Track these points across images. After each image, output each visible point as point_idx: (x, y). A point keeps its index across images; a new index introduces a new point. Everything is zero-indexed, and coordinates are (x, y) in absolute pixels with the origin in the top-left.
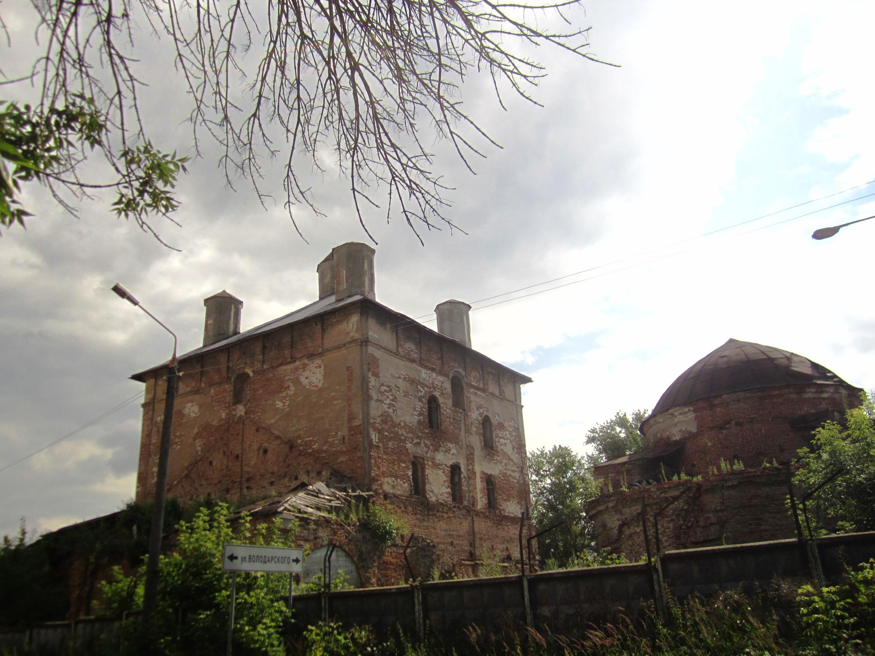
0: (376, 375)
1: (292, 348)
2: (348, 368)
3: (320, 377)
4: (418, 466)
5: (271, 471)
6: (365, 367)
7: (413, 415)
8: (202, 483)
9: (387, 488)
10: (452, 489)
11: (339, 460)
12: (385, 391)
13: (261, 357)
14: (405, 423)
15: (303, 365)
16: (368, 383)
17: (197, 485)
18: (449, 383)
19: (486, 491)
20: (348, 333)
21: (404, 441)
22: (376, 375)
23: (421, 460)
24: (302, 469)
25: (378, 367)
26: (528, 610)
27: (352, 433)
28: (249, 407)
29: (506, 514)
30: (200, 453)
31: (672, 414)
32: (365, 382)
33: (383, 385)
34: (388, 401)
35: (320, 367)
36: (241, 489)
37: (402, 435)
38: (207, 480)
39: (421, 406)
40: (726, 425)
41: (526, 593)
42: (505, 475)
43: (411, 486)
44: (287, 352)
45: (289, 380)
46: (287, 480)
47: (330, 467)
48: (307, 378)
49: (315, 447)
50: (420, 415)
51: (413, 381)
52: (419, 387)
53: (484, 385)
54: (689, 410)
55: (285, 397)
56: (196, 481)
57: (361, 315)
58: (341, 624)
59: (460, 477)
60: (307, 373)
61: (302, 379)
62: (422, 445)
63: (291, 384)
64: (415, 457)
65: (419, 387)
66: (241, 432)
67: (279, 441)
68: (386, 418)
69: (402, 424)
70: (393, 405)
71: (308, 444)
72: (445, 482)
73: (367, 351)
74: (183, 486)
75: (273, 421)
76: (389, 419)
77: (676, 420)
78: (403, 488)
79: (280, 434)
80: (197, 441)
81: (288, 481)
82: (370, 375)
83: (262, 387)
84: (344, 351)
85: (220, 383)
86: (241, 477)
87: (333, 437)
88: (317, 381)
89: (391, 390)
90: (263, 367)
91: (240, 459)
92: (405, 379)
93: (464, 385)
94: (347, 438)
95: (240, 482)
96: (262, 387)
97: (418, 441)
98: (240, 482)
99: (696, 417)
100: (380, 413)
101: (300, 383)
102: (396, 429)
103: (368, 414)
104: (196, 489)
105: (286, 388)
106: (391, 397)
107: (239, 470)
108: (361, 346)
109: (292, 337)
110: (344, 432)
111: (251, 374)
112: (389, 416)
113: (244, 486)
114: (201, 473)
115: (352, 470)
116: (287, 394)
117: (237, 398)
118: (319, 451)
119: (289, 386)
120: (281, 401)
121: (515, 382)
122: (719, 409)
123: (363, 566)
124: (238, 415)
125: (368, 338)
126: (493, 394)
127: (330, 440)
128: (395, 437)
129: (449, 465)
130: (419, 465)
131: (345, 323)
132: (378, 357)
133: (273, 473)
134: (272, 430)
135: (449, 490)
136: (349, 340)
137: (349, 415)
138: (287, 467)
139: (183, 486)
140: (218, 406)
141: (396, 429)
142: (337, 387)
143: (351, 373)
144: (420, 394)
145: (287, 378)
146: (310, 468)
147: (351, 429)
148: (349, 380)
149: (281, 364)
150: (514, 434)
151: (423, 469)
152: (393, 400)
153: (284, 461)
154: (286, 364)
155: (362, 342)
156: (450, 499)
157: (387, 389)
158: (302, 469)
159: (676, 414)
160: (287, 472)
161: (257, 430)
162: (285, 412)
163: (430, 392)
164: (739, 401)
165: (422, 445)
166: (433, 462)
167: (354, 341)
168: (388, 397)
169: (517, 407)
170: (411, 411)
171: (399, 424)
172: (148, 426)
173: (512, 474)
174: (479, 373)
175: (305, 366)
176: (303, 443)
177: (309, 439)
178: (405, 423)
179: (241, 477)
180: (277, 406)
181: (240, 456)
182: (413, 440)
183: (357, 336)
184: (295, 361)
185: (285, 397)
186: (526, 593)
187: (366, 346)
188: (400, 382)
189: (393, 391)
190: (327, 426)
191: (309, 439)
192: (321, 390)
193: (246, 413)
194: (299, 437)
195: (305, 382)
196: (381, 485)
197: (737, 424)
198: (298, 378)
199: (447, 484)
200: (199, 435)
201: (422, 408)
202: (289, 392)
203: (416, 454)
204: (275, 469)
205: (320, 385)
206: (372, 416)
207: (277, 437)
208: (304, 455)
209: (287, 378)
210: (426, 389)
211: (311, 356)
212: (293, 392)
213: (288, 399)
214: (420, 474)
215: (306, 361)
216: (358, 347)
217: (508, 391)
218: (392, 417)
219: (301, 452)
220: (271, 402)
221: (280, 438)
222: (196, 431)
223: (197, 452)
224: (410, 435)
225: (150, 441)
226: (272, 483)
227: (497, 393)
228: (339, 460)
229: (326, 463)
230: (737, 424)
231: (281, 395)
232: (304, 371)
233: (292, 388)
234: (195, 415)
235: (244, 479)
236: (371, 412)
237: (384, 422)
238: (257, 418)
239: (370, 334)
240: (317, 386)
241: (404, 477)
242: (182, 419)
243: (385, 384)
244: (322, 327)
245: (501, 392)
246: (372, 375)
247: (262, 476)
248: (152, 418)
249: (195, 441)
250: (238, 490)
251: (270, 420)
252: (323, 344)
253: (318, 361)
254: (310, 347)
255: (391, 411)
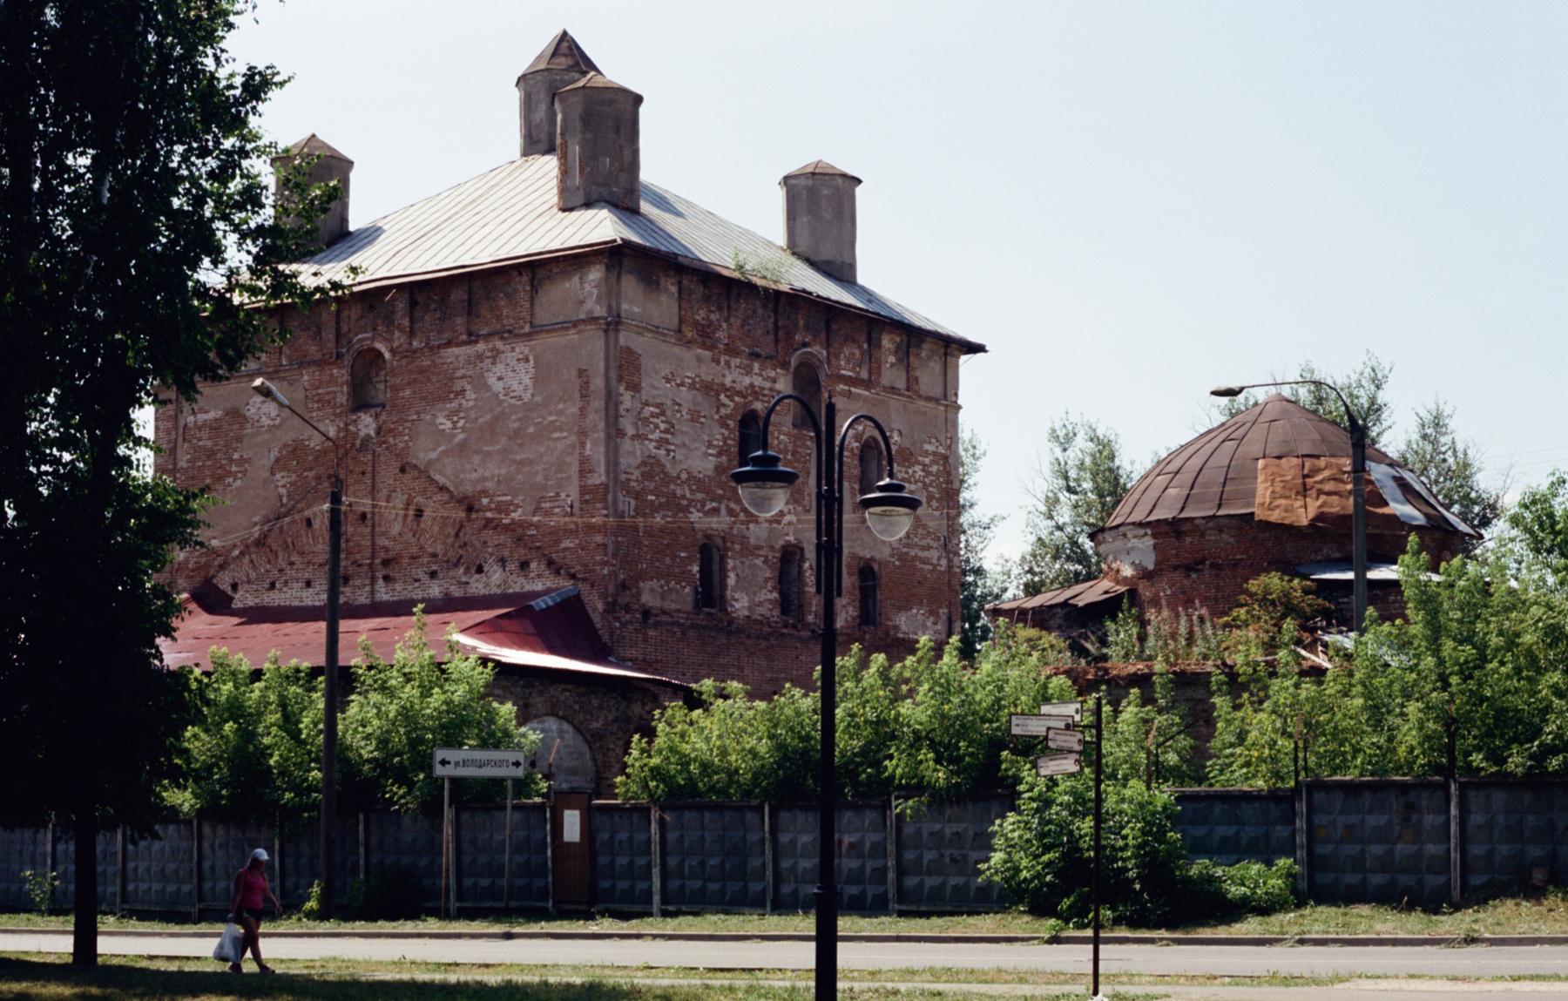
0: (635, 388)
1: (469, 313)
2: (581, 373)
3: (527, 380)
4: (711, 554)
5: (431, 550)
6: (613, 374)
7: (706, 455)
8: (293, 559)
9: (647, 598)
10: (781, 594)
11: (563, 546)
12: (653, 415)
13: (406, 323)
14: (688, 473)
15: (491, 350)
16: (618, 404)
17: (282, 563)
18: (789, 378)
19: (857, 592)
20: (583, 302)
21: (686, 510)
22: (635, 388)
23: (719, 542)
24: (491, 555)
25: (638, 369)
26: (767, 835)
27: (587, 497)
28: (384, 422)
29: (901, 636)
30: (285, 500)
31: (1125, 535)
32: (611, 399)
33: (647, 404)
34: (657, 435)
35: (527, 360)
36: (373, 580)
37: (683, 497)
38: (302, 554)
39: (721, 435)
40: (1197, 564)
41: (767, 819)
42: (903, 558)
43: (697, 592)
44: (459, 320)
45: (464, 377)
46: (462, 571)
47: (544, 555)
48: (500, 379)
49: (516, 515)
50: (719, 454)
51: (710, 390)
52: (722, 396)
53: (870, 373)
54: (1146, 534)
55: (456, 412)
56: (280, 554)
57: (608, 269)
58: (6, 503)
59: (800, 567)
60: (499, 369)
61: (492, 380)
62: (723, 511)
63: (468, 387)
64: (708, 537)
65: (722, 396)
66: (370, 469)
67: (446, 497)
68: (651, 468)
69: (684, 476)
70: (667, 441)
71: (503, 508)
72: (766, 580)
73: (617, 339)
74: (252, 561)
75: (433, 455)
76: (657, 469)
77: (1130, 545)
78: (683, 597)
79: (448, 484)
80: (278, 476)
81: (465, 573)
82: (622, 389)
83: (409, 384)
84: (573, 336)
85: (321, 364)
86: (373, 557)
87: (552, 500)
88: (521, 387)
89: (663, 413)
90: (410, 344)
91: (369, 522)
92: (692, 386)
93: (822, 378)
94: (577, 505)
95: (371, 566)
96: (409, 384)
97: (714, 505)
98: (371, 566)
99: (1155, 547)
100: (639, 461)
101: (487, 387)
102: (672, 487)
103: (616, 464)
104: (281, 571)
105: (457, 394)
106: (663, 426)
107: (369, 543)
108: (606, 331)
109: (470, 293)
110: (571, 494)
111: (387, 355)
112: (659, 463)
113: (379, 575)
114: (289, 540)
115: (586, 566)
116: (460, 405)
117: (360, 403)
118: (521, 524)
119: (464, 391)
120: (448, 417)
121: (946, 354)
122: (1188, 540)
123: (601, 747)
124: (362, 434)
125: (619, 316)
126: (892, 390)
127: (543, 505)
128: (667, 503)
129: (778, 547)
130: (715, 551)
131: (576, 279)
132: (639, 351)
133: (434, 555)
134: (432, 473)
135: (775, 595)
136: (582, 316)
137: (582, 463)
138: (460, 547)
139: (252, 561)
140: (319, 409)
141: (672, 487)
142: (560, 406)
143: (587, 383)
144: (723, 411)
145: (459, 373)
146: (506, 554)
147: (584, 490)
148: (583, 396)
149: (449, 344)
150: (934, 469)
151: (723, 559)
152: (666, 431)
153: (457, 535)
154: (458, 345)
155: (608, 324)
156: (776, 612)
157: (657, 411)
158: (491, 555)
159: (1129, 535)
160: (461, 557)
161: (403, 470)
162: (456, 440)
163: (746, 404)
164: (1221, 531)
165: (723, 511)
166: (742, 544)
167: (593, 320)
168: (657, 427)
169: (947, 401)
170: (703, 449)
171: (678, 477)
172: (168, 432)
173: (920, 554)
174: (860, 347)
175: (496, 355)
176: (493, 506)
177: (505, 498)
178: (689, 473)
179: (373, 557)
180: (442, 427)
181: (369, 516)
182: (703, 505)
183: (599, 311)
184: (476, 342)
185: (456, 412)
186: (767, 819)
187: (617, 331)
188: (685, 395)
189: (669, 413)
190: (539, 479)
191: (505, 498)
192: (529, 407)
193: (378, 433)
194: (485, 493)
195: (498, 387)
196: (638, 595)
197: (1213, 566)
198: (481, 376)
199: (770, 585)
200: (279, 465)
201: (725, 439)
202: (464, 402)
203: (709, 532)
204: (439, 548)
205: (527, 397)
206: (623, 468)
207: (442, 489)
208: (495, 528)
209: (459, 373)
210: (737, 399)
211: (509, 334)
212: (471, 403)
213: (462, 415)
214: (716, 567)
215: (499, 344)
216: (601, 334)
217: (928, 379)
218: (664, 466)
219: (488, 521)
220: (428, 417)
221: (447, 490)
222: (274, 454)
223: (281, 497)
224: (700, 496)
225: (175, 464)
226: (433, 575)
227: (901, 384)
228: (563, 546)
229: (538, 548)
230: (1213, 566)
231: (448, 406)
232: (494, 363)
233: (470, 395)
234: (269, 422)
235: (378, 561)
236: (622, 460)
237: (648, 476)
238: (401, 445)
239: (624, 306)
240: (520, 398)
241: (685, 576)
242: (242, 427)
243: (651, 400)
244: (532, 280)
245: (912, 382)
246: (626, 389)
247: (413, 558)
248: (176, 418)
249: (273, 474)
250: (367, 582)
251: (424, 453)
252: (532, 315)
253: (522, 348)
254: (508, 317)
255: (663, 452)
